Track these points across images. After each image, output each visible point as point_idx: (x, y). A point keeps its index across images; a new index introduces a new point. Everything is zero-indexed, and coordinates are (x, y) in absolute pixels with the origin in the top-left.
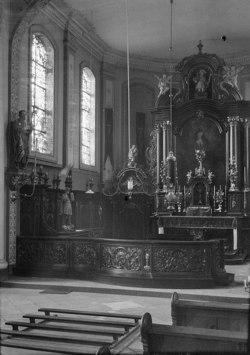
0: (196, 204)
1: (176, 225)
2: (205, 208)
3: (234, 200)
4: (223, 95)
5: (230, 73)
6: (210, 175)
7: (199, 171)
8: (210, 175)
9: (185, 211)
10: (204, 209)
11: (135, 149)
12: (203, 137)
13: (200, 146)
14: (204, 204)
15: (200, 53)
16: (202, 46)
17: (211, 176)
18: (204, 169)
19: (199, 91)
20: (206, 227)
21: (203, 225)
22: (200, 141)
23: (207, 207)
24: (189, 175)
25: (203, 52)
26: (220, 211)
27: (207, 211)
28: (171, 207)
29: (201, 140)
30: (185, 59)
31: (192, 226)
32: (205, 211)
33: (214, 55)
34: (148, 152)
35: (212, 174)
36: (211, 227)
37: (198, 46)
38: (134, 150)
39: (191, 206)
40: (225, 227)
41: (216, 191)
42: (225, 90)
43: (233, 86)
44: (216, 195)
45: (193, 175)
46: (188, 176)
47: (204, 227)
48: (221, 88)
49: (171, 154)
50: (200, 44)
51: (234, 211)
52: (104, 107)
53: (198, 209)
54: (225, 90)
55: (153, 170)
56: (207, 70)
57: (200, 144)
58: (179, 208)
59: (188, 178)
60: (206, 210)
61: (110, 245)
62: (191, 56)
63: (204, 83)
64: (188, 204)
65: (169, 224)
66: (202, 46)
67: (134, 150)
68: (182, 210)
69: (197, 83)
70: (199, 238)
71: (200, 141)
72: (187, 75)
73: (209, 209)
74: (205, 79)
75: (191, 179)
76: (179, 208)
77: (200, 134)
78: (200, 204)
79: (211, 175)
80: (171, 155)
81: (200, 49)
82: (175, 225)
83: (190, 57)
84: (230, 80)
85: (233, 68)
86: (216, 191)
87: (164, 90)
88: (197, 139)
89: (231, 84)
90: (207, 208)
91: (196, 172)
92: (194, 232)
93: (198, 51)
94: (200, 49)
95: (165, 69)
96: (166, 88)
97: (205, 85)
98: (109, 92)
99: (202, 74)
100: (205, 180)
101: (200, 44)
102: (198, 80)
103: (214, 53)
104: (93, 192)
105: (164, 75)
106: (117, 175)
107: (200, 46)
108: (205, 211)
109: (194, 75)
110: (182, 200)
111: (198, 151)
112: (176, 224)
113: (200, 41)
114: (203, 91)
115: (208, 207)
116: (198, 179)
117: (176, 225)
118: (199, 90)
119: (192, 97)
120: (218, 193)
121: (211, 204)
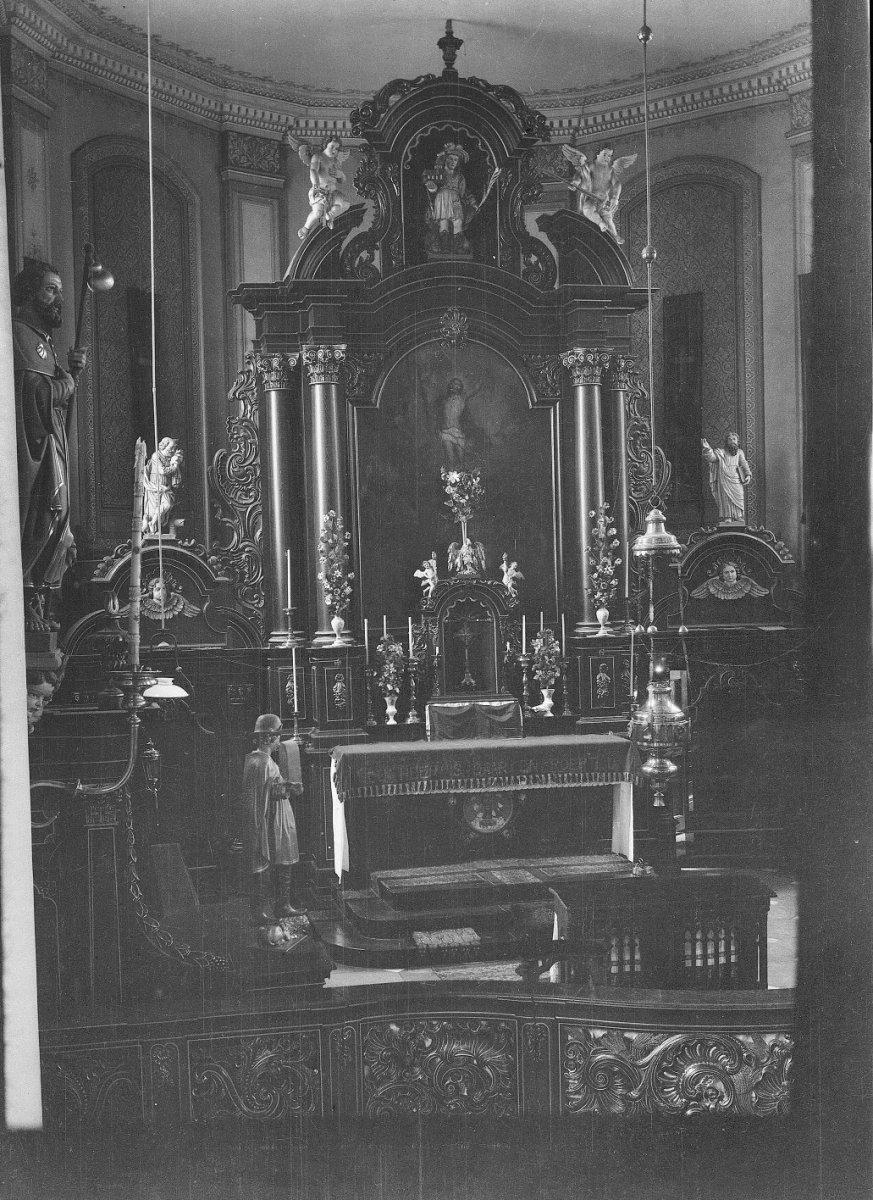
0: (455, 690)
1: (411, 786)
2: (495, 704)
3: (604, 670)
4: (534, 259)
5: (591, 174)
6: (509, 575)
7: (465, 555)
8: (509, 575)
9: (416, 720)
10: (491, 710)
11: (173, 454)
12: (465, 419)
13: (455, 450)
14: (483, 688)
15: (450, 73)
16: (458, 43)
17: (514, 579)
18: (480, 548)
19: (442, 230)
20: (528, 783)
21: (518, 777)
22: (452, 435)
23: (499, 698)
24: (428, 574)
25: (464, 67)
26: (550, 715)
27: (506, 718)
28: (662, 767)
29: (456, 432)
30: (396, 86)
31: (475, 786)
32: (497, 718)
33: (508, 92)
34: (222, 469)
35: (516, 570)
36: (547, 781)
37: (442, 44)
38: (168, 459)
39: (440, 700)
40: (600, 780)
41: (531, 635)
42: (543, 237)
43: (603, 227)
44: (530, 649)
45: (443, 570)
46: (425, 578)
47: (523, 786)
48: (528, 229)
49: (657, 521)
50: (450, 33)
51: (607, 713)
52: (21, 255)
53: (472, 710)
54: (543, 237)
55: (245, 546)
56: (470, 145)
57: (455, 447)
58: (391, 710)
59: (424, 583)
60: (503, 711)
61: (573, 1022)
62: (419, 78)
63: (463, 199)
64: (425, 695)
65: (380, 785)
66: (458, 43)
67: (168, 459)
68: (401, 716)
69: (434, 196)
70: (495, 828)
71: (452, 435)
72: (392, 158)
73: (512, 709)
74: (464, 182)
75: (438, 587)
76: (391, 710)
77: (454, 407)
78: (468, 689)
79: (515, 574)
80: (658, 530)
81: (449, 59)
82: (407, 785)
83: (413, 83)
84: (590, 200)
85: (603, 156)
86: (531, 635)
87: (329, 209)
88: (442, 424)
89: (594, 218)
90: (506, 703)
91: (453, 561)
92: (476, 807)
93: (443, 66)
94: (449, 59)
95: (221, 114)
96: (336, 203)
97: (467, 209)
98: (33, 182)
99: (455, 161)
100: (488, 593)
101: (450, 33)
102: (440, 186)
103: (506, 83)
104: (179, 692)
105: (330, 145)
106: (96, 572)
107: (449, 44)
108: (497, 718)
109: (427, 155)
110: (403, 676)
111: (454, 477)
112: (414, 777)
113: (449, 22)
114: (457, 230)
115: (506, 698)
116: (468, 587)
117: (411, 786)
118: (443, 226)
119: (417, 252)
120: (538, 644)
121: (515, 689)
